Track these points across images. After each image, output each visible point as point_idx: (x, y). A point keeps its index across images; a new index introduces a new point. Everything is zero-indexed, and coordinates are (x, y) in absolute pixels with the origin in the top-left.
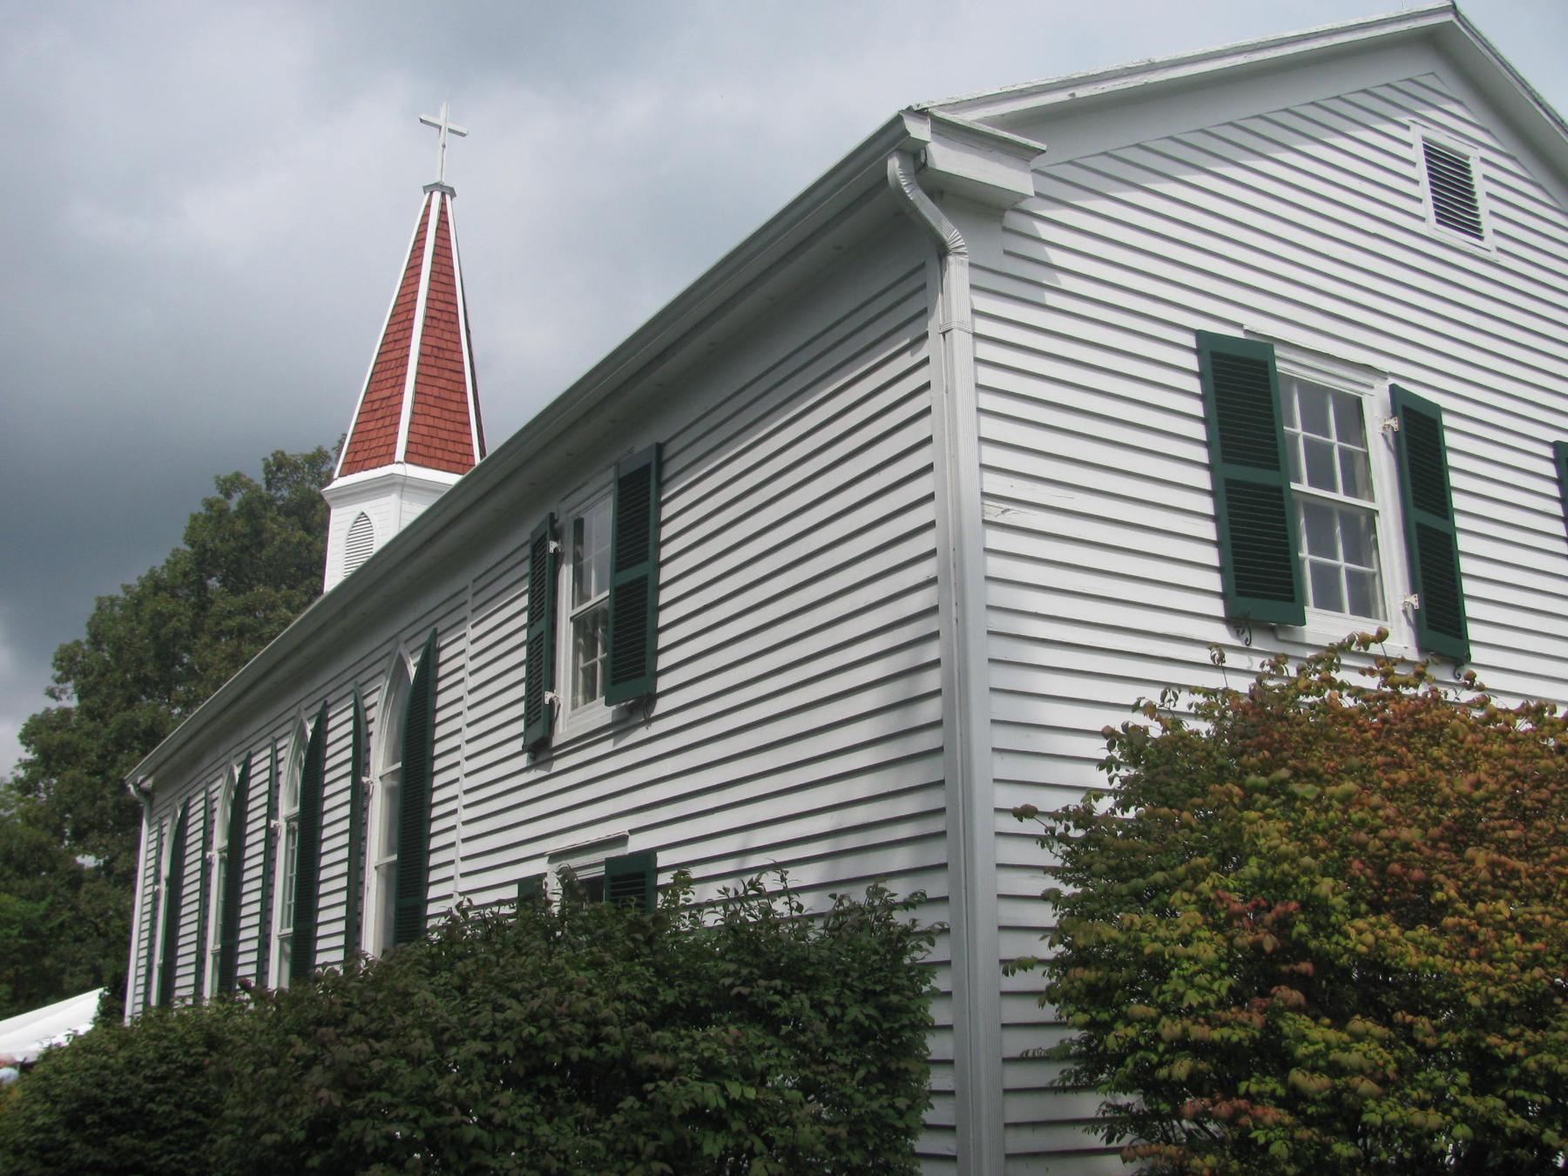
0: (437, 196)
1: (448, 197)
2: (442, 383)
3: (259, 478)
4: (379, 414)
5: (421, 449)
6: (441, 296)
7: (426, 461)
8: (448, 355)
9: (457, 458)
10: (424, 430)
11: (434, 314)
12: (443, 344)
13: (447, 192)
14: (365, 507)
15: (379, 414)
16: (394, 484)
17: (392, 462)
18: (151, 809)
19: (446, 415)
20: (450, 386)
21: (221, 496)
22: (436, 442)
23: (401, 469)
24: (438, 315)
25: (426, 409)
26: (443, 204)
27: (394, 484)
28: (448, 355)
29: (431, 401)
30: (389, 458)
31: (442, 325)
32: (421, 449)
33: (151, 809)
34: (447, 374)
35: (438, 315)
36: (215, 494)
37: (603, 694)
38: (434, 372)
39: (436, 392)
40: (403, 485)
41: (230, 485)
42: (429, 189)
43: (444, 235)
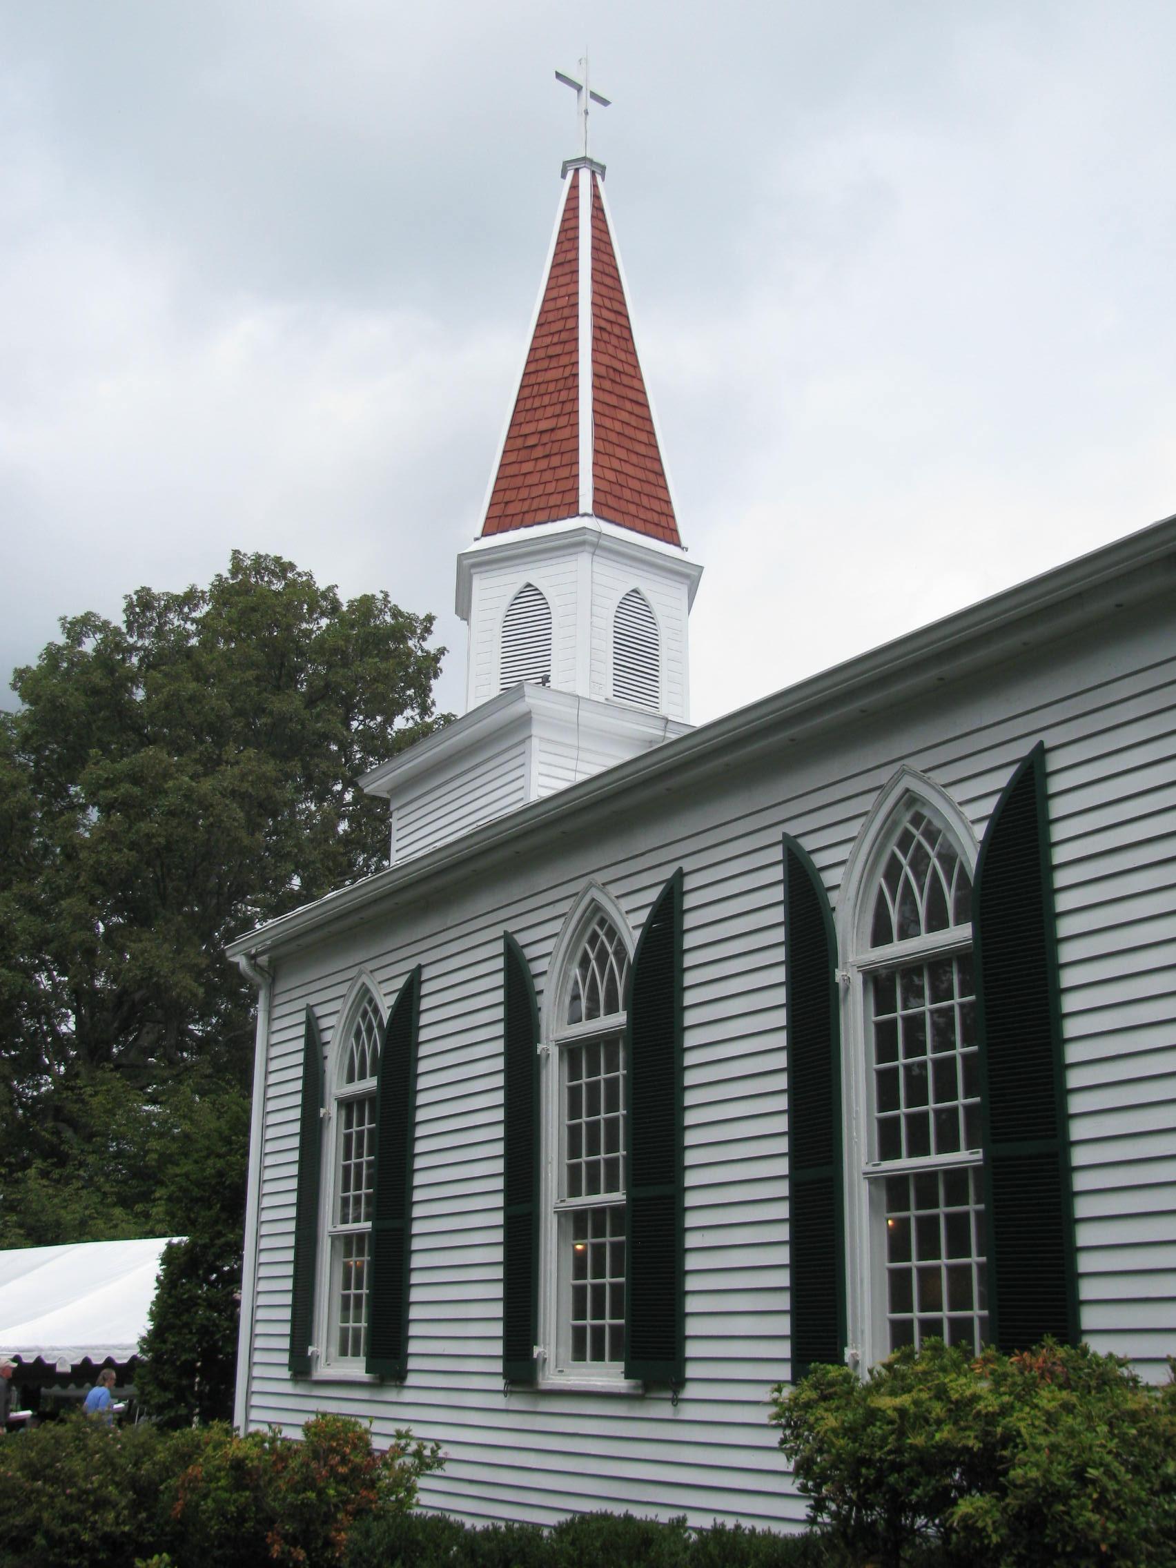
0: (585, 177)
1: (599, 178)
2: (624, 416)
3: (118, 620)
4: (538, 452)
5: (611, 501)
6: (608, 303)
7: (619, 517)
8: (626, 380)
9: (656, 517)
10: (611, 476)
11: (603, 324)
12: (619, 366)
13: (598, 170)
14: (540, 575)
15: (538, 452)
16: (583, 543)
17: (577, 514)
18: (271, 997)
19: (634, 459)
20: (633, 421)
21: (124, 630)
22: (627, 494)
23: (585, 521)
24: (608, 326)
25: (610, 449)
26: (595, 186)
27: (583, 543)
28: (626, 380)
29: (613, 437)
30: (572, 510)
31: (614, 341)
32: (611, 501)
33: (271, 997)
34: (628, 406)
35: (608, 326)
36: (61, 640)
37: (365, 1355)
38: (613, 400)
39: (618, 427)
40: (596, 546)
41: (78, 627)
42: (572, 166)
43: (600, 225)
